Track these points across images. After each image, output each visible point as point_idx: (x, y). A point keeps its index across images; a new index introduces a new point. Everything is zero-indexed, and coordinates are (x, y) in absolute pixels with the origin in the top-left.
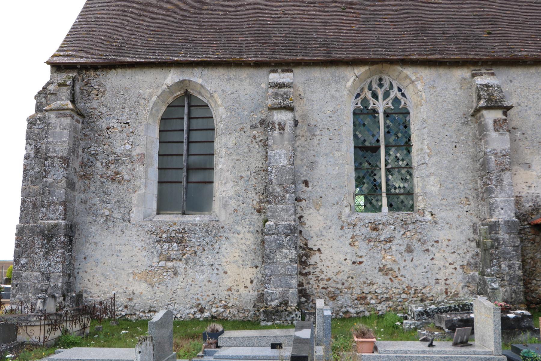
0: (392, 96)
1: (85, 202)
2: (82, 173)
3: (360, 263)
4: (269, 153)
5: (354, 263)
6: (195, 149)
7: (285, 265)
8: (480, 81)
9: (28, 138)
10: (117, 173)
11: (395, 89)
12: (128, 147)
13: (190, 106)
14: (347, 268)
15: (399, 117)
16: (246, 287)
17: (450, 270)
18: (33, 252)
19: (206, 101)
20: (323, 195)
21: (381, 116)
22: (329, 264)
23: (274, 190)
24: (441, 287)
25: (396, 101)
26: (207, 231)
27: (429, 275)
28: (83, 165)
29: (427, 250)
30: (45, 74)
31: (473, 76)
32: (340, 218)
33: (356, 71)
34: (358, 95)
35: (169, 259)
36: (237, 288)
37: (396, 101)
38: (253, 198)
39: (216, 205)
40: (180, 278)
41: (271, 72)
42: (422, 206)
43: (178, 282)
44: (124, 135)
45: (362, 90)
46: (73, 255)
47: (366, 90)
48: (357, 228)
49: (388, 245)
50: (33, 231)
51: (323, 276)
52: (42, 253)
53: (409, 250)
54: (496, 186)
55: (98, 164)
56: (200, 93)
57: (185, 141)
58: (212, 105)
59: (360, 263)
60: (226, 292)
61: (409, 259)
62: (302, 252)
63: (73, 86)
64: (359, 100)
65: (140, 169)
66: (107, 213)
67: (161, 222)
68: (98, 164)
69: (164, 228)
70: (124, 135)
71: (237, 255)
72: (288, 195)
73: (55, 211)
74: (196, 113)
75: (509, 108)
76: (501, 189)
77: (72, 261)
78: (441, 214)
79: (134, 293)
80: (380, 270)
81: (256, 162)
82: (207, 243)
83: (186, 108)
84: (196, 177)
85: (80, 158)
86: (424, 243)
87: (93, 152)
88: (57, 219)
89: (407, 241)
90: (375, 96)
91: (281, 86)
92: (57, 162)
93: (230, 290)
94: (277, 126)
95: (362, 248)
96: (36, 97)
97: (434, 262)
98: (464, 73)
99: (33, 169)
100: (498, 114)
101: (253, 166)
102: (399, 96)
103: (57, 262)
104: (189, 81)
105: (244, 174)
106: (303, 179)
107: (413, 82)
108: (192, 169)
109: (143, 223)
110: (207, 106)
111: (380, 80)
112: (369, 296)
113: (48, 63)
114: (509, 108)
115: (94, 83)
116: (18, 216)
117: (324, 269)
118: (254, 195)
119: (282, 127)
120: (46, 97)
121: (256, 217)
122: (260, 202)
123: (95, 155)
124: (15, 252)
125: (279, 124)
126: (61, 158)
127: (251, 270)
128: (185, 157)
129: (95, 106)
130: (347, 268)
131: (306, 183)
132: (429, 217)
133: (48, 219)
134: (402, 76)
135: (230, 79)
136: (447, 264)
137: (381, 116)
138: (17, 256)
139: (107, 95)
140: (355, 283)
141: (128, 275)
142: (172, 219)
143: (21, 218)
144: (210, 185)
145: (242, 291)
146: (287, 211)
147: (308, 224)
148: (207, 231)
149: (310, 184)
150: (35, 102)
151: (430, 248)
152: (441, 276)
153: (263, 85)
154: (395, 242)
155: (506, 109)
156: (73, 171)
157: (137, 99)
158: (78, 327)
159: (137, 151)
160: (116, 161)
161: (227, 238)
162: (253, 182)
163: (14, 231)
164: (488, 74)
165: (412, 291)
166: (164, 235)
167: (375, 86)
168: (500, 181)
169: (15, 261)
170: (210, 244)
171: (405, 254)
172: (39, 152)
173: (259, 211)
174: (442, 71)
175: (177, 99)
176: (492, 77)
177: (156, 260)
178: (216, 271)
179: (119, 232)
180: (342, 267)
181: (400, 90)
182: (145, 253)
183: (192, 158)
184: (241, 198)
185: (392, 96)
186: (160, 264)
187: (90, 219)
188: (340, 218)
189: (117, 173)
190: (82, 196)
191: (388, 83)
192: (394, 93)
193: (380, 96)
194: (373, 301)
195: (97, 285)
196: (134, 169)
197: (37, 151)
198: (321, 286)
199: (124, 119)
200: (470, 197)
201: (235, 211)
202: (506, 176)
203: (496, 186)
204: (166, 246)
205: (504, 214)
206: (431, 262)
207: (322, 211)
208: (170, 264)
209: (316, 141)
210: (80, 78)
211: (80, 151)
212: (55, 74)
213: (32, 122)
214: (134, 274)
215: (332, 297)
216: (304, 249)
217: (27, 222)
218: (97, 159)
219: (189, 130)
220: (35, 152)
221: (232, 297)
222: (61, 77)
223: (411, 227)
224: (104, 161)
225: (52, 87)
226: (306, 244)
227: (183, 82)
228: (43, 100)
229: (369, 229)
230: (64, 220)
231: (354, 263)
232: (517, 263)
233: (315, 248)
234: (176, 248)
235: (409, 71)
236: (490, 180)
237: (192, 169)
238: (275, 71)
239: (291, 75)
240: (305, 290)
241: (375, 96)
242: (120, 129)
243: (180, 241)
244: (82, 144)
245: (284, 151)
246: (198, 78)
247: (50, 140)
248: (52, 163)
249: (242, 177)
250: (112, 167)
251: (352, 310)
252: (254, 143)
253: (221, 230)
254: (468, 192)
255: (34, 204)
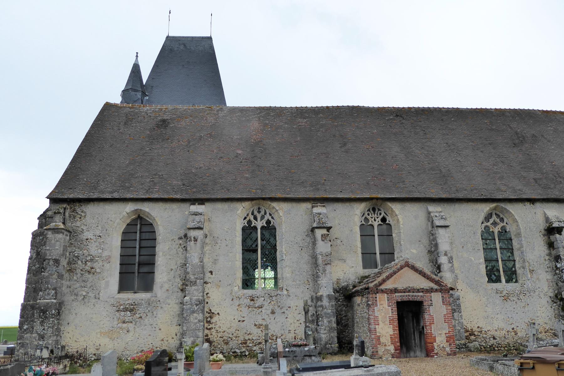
0: (266, 219)
1: (70, 287)
2: (68, 268)
3: (243, 321)
4: (188, 255)
5: (239, 321)
6: (144, 252)
7: (196, 324)
8: (316, 210)
9: (32, 245)
10: (92, 268)
11: (268, 214)
12: (100, 251)
13: (141, 225)
14: (235, 324)
15: (270, 230)
16: (173, 338)
17: (297, 324)
18: (32, 321)
19: (151, 222)
20: (221, 280)
21: (259, 231)
22: (223, 322)
23: (190, 278)
24: (292, 335)
25: (268, 222)
26: (149, 304)
27: (284, 327)
28: (69, 263)
29: (284, 313)
30: (46, 204)
31: (313, 207)
32: (231, 293)
33: (243, 204)
34: (245, 218)
35: (124, 322)
36: (167, 339)
37: (268, 222)
38: (178, 282)
39: (156, 287)
40: (131, 334)
41: (191, 205)
42: (282, 286)
43: (129, 337)
44: (97, 244)
45: (248, 215)
46: (60, 322)
47: (250, 215)
48: (241, 300)
49: (260, 310)
50: (33, 307)
51: (220, 330)
52: (39, 322)
53: (273, 312)
54: (322, 274)
55: (79, 262)
56: (148, 217)
57: (138, 247)
58: (155, 225)
59: (243, 321)
60: (160, 342)
61: (272, 318)
62: (208, 315)
63: (64, 213)
64: (246, 221)
65: (107, 266)
66: (84, 294)
67: (120, 299)
68: (79, 262)
69: (122, 302)
70: (97, 244)
71: (167, 318)
72: (198, 281)
73: (49, 294)
74: (145, 229)
75: (330, 228)
76: (325, 276)
77: (60, 326)
78: (292, 290)
79: (100, 345)
80: (255, 325)
81: (180, 261)
82: (149, 311)
83: (139, 226)
84: (145, 269)
85: (68, 259)
86: (281, 308)
87: (76, 255)
88: (51, 299)
89: (271, 307)
90: (255, 218)
91: (196, 214)
92: (51, 262)
93: (163, 340)
94: (193, 239)
95: (245, 311)
96: (38, 218)
97: (287, 319)
98: (308, 205)
99: (34, 266)
100: (324, 231)
101: (179, 263)
102: (270, 218)
103: (49, 327)
104: (141, 210)
105: (173, 268)
106: (210, 270)
107: (277, 211)
108: (142, 264)
109: (108, 300)
110: (152, 224)
111: (259, 208)
112: (249, 342)
113: (47, 198)
114: (330, 228)
115: (79, 210)
116: (23, 297)
117: (221, 325)
118: (179, 280)
119: (196, 240)
120: (45, 219)
121: (180, 294)
122: (183, 284)
123: (77, 257)
124: (20, 320)
125: (194, 238)
126: (54, 259)
127: (176, 327)
128: (137, 257)
129: (79, 225)
130: (235, 324)
131: (211, 272)
132: (285, 292)
133: (44, 299)
134: (271, 207)
135: (166, 209)
136: (296, 321)
137: (259, 231)
138: (21, 324)
139: (87, 218)
140: (240, 334)
141: (97, 333)
142: (129, 297)
143: (24, 299)
144: (151, 274)
145: (171, 341)
146: (197, 290)
147: (212, 297)
148: (149, 304)
149: (214, 273)
150: (38, 221)
151: (285, 311)
152: (292, 328)
153: (187, 213)
154: (264, 308)
155: (329, 229)
156: (62, 267)
157: (105, 228)
158: (61, 366)
159: (106, 254)
160: (91, 260)
161: (161, 308)
162: (179, 272)
163: (19, 308)
164: (321, 206)
165: (274, 338)
166: (122, 307)
167: (256, 213)
168: (325, 271)
169: (19, 327)
170: (151, 311)
171: (271, 315)
172: (39, 254)
173: (182, 290)
174: (294, 204)
175: (133, 220)
176: (323, 208)
177: (116, 323)
178: (154, 329)
179: (92, 306)
180: (232, 324)
181: (270, 215)
182: (108, 319)
183: (142, 257)
184: (171, 283)
185: (266, 219)
186: (118, 326)
187: (73, 298)
188: (231, 293)
189: (92, 268)
190: (68, 283)
191: (264, 211)
192: (267, 217)
193: (259, 219)
194: (251, 345)
195: (76, 341)
196: (103, 266)
197: (38, 254)
198: (219, 336)
199: (98, 233)
200: (310, 280)
201: (167, 290)
202: (328, 267)
203: (322, 274)
204: (122, 313)
205: (326, 290)
206: (286, 320)
207: (220, 289)
208: (125, 325)
209: (218, 247)
210: (69, 207)
211: (68, 254)
212: (52, 205)
213: (35, 235)
214: (101, 333)
215: (226, 343)
216: (209, 313)
217: (29, 301)
218: (79, 259)
219: (141, 240)
220: (36, 255)
221: (164, 344)
222: (57, 207)
223: (274, 298)
224: (84, 260)
225: (50, 213)
226: (210, 310)
227: (136, 210)
228: (44, 221)
229: (249, 300)
230: (55, 299)
231: (239, 321)
232: (334, 319)
233: (216, 313)
234: (130, 315)
235: (275, 204)
236: (319, 270)
237: (142, 264)
238: (194, 204)
239: (203, 206)
240: (209, 339)
241: (255, 218)
242: (95, 240)
243: (131, 310)
244: (69, 249)
245: (197, 254)
246: (146, 207)
247: (48, 248)
248: (49, 263)
249: (172, 270)
250: (89, 264)
251: (238, 351)
252: (180, 248)
253: (158, 303)
254: (309, 276)
255: (35, 289)
